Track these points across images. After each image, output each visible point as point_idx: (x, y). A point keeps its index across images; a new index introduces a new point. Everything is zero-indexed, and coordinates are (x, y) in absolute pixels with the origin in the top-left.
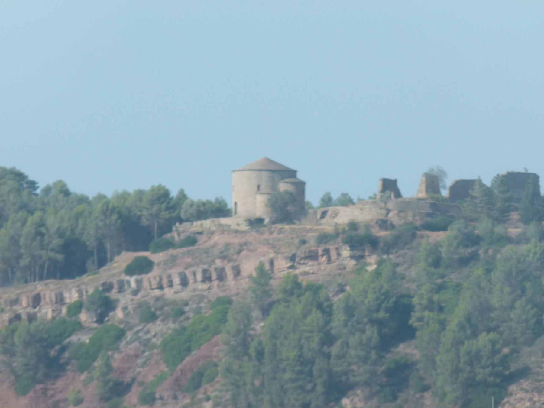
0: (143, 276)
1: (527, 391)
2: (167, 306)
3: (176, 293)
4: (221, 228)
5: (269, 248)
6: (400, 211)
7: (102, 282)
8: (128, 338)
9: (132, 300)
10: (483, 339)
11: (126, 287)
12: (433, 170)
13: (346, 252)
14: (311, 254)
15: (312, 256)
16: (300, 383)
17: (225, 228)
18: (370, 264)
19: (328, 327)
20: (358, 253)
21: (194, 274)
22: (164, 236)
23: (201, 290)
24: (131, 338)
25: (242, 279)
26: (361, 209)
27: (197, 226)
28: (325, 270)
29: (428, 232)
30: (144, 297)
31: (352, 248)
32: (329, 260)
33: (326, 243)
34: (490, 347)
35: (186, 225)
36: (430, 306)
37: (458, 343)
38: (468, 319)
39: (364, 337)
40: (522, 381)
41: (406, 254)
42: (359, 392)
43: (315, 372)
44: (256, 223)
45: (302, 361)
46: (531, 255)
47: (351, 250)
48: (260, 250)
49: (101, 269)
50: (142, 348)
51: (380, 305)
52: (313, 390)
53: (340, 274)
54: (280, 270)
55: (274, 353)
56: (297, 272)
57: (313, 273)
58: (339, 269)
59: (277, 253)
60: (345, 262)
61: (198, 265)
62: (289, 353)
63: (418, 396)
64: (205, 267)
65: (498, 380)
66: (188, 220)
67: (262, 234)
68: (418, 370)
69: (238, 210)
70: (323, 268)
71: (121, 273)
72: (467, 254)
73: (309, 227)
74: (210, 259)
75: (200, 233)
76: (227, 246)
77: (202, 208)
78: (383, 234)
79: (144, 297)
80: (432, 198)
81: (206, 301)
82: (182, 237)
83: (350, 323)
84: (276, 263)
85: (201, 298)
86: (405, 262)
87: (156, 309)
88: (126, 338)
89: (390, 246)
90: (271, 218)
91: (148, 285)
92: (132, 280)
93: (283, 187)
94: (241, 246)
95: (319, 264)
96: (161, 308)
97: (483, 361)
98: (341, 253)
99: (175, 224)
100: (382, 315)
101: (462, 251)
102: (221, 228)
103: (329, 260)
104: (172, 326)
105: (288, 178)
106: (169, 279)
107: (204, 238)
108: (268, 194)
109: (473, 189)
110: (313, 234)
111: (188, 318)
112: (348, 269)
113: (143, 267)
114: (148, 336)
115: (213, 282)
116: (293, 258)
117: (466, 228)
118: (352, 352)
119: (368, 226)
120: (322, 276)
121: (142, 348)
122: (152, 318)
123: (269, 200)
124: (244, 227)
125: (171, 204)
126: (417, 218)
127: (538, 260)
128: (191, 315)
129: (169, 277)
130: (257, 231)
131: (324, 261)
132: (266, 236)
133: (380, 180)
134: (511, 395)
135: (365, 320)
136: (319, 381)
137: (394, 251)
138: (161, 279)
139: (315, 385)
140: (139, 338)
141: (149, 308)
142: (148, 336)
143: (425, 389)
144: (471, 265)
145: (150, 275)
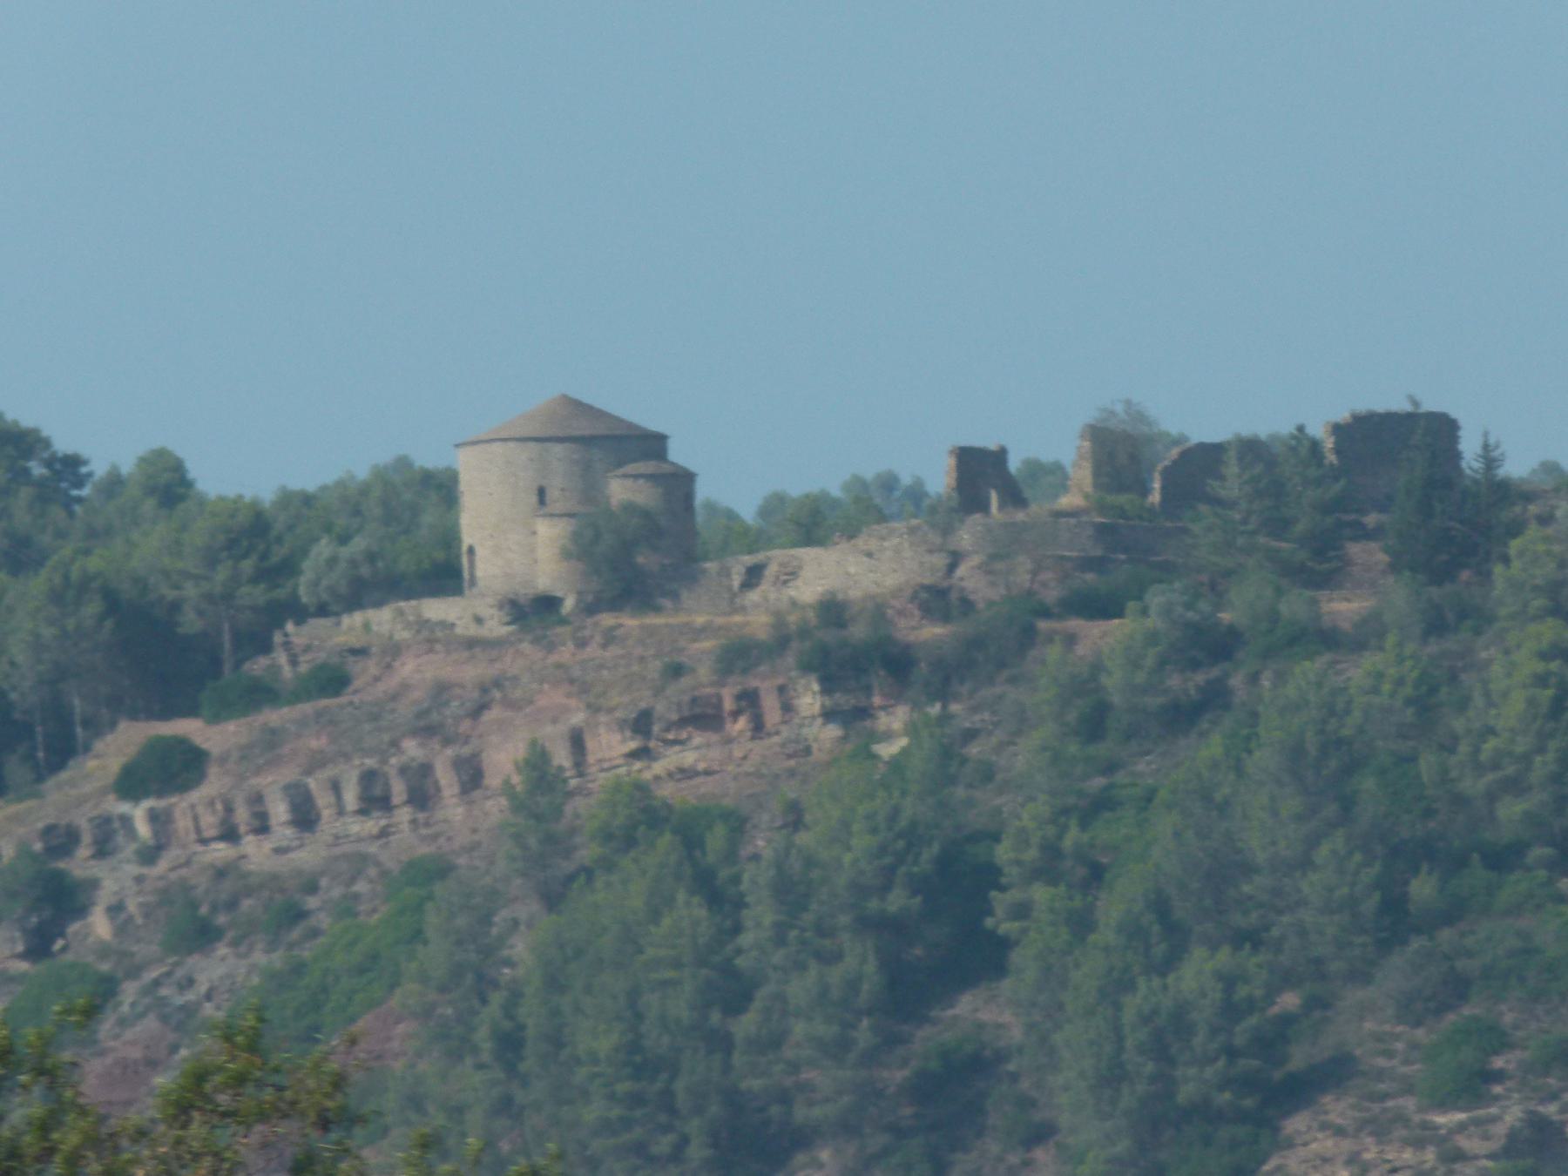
0: (173, 800)
1: (1340, 1132)
2: (248, 895)
3: (279, 851)
4: (425, 634)
5: (569, 695)
6: (994, 557)
7: (40, 825)
8: (125, 1008)
9: (139, 879)
10: (1197, 974)
11: (120, 839)
12: (1113, 413)
13: (810, 700)
14: (698, 710)
15: (704, 717)
16: (637, 1133)
17: (439, 634)
18: (888, 736)
19: (729, 949)
20: (844, 700)
21: (336, 787)
22: (247, 666)
23: (360, 840)
24: (133, 1005)
25: (488, 798)
26: (870, 555)
27: (351, 629)
28: (745, 758)
29: (1074, 624)
30: (180, 866)
31: (829, 684)
32: (758, 728)
33: (745, 671)
34: (1218, 995)
35: (318, 625)
36: (1048, 868)
37: (1117, 986)
38: (1160, 906)
39: (836, 975)
40: (1327, 1099)
41: (1000, 697)
42: (825, 1155)
43: (682, 1100)
44: (533, 611)
45: (638, 1060)
46: (1387, 687)
47: (826, 690)
48: (542, 702)
49: (50, 783)
50: (172, 1037)
51: (890, 871)
52: (677, 1155)
53: (792, 773)
54: (606, 765)
55: (556, 1041)
56: (658, 768)
57: (707, 773)
58: (790, 756)
59: (594, 709)
60: (810, 732)
61: (347, 757)
62: (597, 1040)
63: (1014, 1159)
64: (370, 762)
65: (1249, 1103)
66: (322, 611)
67: (551, 647)
68: (1014, 1078)
69: (479, 573)
70: (738, 753)
71: (103, 792)
72: (1192, 692)
73: (700, 620)
74: (386, 737)
75: (360, 652)
76: (441, 690)
77: (365, 571)
78: (933, 632)
79: (180, 866)
80: (1102, 508)
81: (372, 872)
82: (303, 668)
83: (793, 934)
84: (590, 744)
85: (360, 862)
86: (996, 725)
87: (214, 909)
88: (120, 1004)
89: (949, 674)
90: (580, 593)
91: (190, 824)
92: (139, 814)
93: (621, 490)
94: (484, 690)
95: (729, 741)
96: (232, 905)
97: (1198, 1040)
98: (796, 702)
99: (281, 626)
100: (897, 901)
101: (1174, 681)
102: (425, 634)
103: (758, 728)
104: (259, 958)
105: (635, 460)
106: (262, 807)
107: (372, 667)
108: (570, 515)
109: (1222, 478)
110: (707, 644)
111: (315, 933)
112: (818, 755)
113: (172, 769)
114: (190, 996)
115: (397, 812)
116: (641, 724)
117: (1189, 606)
118: (799, 1029)
119: (878, 611)
120: (735, 778)
121: (172, 1037)
122: (201, 935)
123: (576, 536)
124: (497, 626)
125: (275, 559)
126: (1047, 576)
127: (1409, 702)
128: (323, 920)
129: (257, 799)
130: (536, 641)
131: (741, 732)
132: (566, 653)
133: (951, 452)
134: (1290, 1145)
135: (844, 919)
136: (694, 1126)
137: (965, 689)
138: (229, 810)
139: (685, 1141)
140: (162, 1002)
141: (194, 906)
142: (190, 996)
143: (1041, 1134)
144: (1205, 726)
145: (195, 796)
